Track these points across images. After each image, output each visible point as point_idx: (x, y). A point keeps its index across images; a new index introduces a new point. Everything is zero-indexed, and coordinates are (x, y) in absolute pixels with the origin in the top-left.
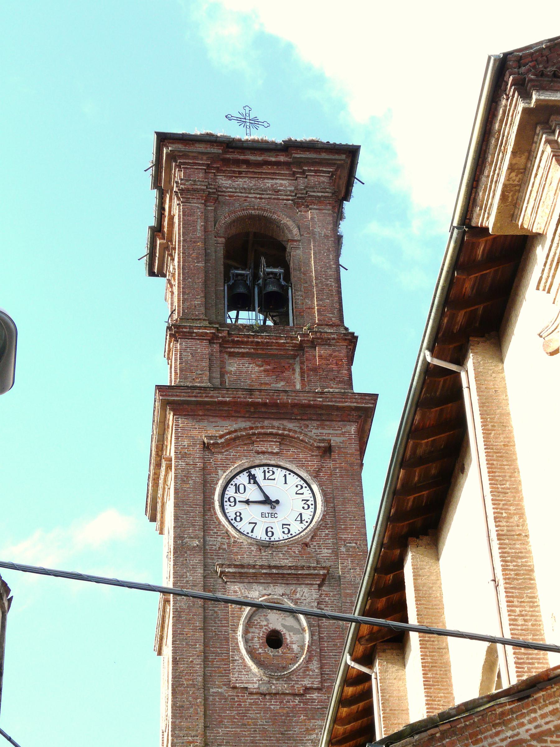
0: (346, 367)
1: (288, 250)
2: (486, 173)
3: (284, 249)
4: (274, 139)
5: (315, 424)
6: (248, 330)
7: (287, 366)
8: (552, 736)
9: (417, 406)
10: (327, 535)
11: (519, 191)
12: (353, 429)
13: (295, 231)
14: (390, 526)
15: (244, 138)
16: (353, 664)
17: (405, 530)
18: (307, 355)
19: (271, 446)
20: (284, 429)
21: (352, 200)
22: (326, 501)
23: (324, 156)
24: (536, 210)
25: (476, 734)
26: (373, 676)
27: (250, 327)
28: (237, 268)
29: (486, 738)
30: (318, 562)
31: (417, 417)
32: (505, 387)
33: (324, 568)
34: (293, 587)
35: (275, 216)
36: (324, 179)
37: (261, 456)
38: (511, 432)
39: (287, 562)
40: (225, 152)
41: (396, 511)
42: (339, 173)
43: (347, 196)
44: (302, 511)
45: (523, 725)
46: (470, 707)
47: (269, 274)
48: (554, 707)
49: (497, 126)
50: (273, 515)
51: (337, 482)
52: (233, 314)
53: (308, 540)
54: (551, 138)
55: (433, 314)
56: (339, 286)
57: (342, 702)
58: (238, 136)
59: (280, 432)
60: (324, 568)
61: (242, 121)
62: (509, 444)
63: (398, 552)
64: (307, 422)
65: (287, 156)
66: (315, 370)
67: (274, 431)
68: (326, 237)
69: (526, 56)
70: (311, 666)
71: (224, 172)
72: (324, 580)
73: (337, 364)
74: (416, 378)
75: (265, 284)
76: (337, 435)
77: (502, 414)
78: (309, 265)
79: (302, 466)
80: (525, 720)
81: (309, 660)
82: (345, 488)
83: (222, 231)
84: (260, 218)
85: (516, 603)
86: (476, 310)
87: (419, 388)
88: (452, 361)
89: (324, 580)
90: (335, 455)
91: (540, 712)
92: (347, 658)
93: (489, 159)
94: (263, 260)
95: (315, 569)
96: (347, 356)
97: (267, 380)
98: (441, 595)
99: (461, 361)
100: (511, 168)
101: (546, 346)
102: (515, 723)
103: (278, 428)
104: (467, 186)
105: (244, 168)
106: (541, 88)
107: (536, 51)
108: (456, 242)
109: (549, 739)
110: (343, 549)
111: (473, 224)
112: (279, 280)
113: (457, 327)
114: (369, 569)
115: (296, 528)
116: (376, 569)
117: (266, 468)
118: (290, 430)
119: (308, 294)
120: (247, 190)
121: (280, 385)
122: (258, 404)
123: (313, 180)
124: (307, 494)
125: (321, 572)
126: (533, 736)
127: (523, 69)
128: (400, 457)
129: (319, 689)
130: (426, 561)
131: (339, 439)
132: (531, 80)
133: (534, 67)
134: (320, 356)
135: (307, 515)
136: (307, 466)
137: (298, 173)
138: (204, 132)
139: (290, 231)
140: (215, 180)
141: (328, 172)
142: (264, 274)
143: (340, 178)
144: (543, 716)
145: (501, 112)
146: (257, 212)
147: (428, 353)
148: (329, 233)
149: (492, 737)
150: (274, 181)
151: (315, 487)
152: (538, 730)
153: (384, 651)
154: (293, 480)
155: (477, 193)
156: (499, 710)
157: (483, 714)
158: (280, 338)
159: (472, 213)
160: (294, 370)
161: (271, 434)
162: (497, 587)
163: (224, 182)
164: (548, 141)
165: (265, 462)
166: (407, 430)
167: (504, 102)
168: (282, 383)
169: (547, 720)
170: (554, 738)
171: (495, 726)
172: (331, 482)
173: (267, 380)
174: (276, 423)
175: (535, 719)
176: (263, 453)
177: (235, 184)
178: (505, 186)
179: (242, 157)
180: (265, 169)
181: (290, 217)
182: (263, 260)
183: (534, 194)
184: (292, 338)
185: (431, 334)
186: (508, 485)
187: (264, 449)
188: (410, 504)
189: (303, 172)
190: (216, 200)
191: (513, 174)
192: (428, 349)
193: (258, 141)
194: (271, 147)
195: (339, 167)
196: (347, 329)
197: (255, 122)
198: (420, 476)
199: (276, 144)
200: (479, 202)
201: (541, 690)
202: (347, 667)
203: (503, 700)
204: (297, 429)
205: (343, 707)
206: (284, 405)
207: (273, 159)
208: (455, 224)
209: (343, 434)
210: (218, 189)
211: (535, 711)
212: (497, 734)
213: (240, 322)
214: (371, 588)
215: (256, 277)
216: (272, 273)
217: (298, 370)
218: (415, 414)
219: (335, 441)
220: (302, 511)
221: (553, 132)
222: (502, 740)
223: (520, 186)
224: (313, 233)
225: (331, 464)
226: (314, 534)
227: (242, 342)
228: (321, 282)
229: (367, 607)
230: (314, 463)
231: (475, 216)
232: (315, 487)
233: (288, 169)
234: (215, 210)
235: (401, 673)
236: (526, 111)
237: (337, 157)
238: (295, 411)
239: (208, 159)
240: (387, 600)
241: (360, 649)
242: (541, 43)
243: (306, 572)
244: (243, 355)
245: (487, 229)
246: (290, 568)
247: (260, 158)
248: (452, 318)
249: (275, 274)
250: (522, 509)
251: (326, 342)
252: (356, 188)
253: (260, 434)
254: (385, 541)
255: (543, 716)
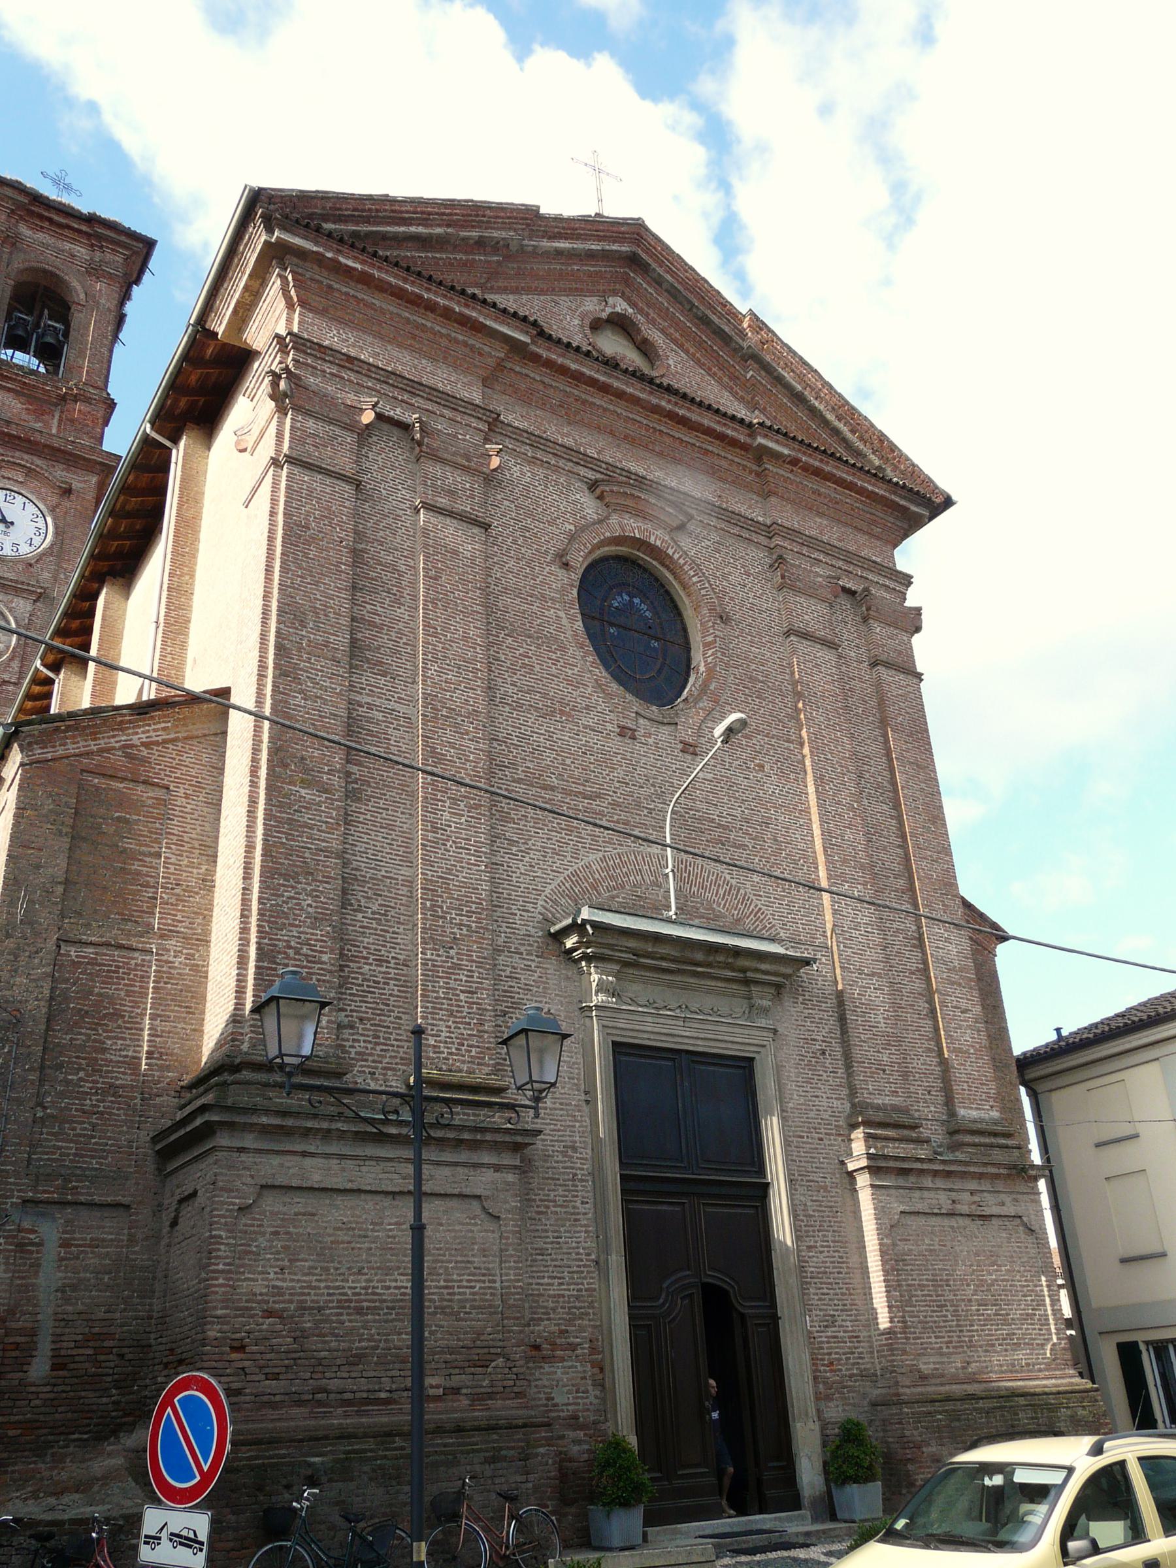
0: (100, 426)
1: (72, 310)
2: (225, 286)
3: (70, 308)
4: (80, 208)
5: (62, 466)
6: (18, 370)
7: (48, 411)
8: (158, 746)
9: (132, 467)
10: (51, 561)
11: (249, 310)
12: (94, 479)
13: (82, 296)
14: (92, 563)
15: (53, 197)
16: (42, 668)
17: (105, 569)
18: (68, 406)
19: (17, 475)
20: (32, 464)
21: (141, 286)
22: (57, 533)
23: (123, 238)
24: (259, 329)
25: (96, 733)
26: (57, 681)
27: (21, 368)
28: (21, 312)
29: (103, 738)
30: (37, 582)
31: (131, 478)
32: (206, 472)
33: (42, 588)
34: (10, 597)
35: (67, 277)
36: (119, 259)
37: (7, 481)
38: (201, 508)
39: (11, 576)
40: (31, 204)
41: (99, 552)
42: (133, 258)
43: (137, 281)
44: (34, 537)
45: (137, 733)
46: (96, 711)
47: (49, 326)
48: (167, 725)
49: (241, 248)
50: (6, 534)
51: (70, 519)
52: (9, 352)
53: (33, 562)
54: (282, 273)
55: (159, 394)
56: (111, 356)
57: (28, 696)
58: (46, 194)
59: (28, 465)
60: (42, 588)
61: (56, 182)
62: (197, 518)
63: (96, 586)
64: (55, 463)
65: (89, 227)
66: (72, 421)
67: (23, 463)
68: (109, 310)
69: (277, 196)
70: (12, 664)
71: (26, 221)
72: (39, 597)
73: (93, 422)
74: (135, 444)
75: (43, 335)
76: (79, 481)
77: (197, 492)
78: (88, 330)
79: (42, 499)
80: (140, 731)
81: (11, 659)
82: (75, 527)
83: (13, 275)
84: (53, 274)
85: (169, 644)
86: (198, 401)
87: (136, 454)
88: (169, 439)
89: (39, 597)
90: (73, 497)
91: (153, 727)
92: (38, 663)
93: (230, 275)
94: (46, 312)
95: (33, 586)
96: (104, 417)
97: (27, 417)
98: (123, 628)
99: (175, 441)
100: (246, 288)
101: (237, 443)
102: (131, 731)
103: (27, 461)
104: (208, 292)
105: (46, 224)
106: (284, 228)
107: (286, 196)
108: (189, 338)
109: (155, 748)
110: (62, 576)
111: (207, 327)
112: (58, 334)
113: (179, 411)
114: (68, 594)
115: (24, 549)
116: (74, 595)
117: (8, 492)
118: (37, 466)
119: (82, 354)
120: (46, 246)
121: (38, 425)
122: (13, 436)
123: (109, 256)
124: (41, 523)
125: (39, 591)
126: (143, 744)
127: (272, 207)
128: (111, 506)
129: (15, 684)
130: (117, 599)
131: (80, 485)
132: (276, 218)
133: (282, 208)
134: (80, 411)
135: (37, 541)
136: (46, 501)
137: (97, 246)
138: (14, 178)
139: (78, 295)
140: (16, 227)
141: (124, 255)
142: (45, 325)
143: (134, 263)
144: (155, 730)
145: (247, 237)
146: (50, 268)
147: (148, 426)
148: (113, 308)
149: (108, 737)
150: (73, 246)
151: (49, 519)
152: (148, 740)
153: (71, 663)
154: (31, 508)
155: (215, 301)
156: (119, 719)
157: (105, 720)
158: (47, 385)
159: (208, 317)
160: (53, 416)
161: (19, 464)
162: (157, 627)
163: (24, 230)
164: (279, 275)
165: (8, 486)
166: (121, 486)
167: (251, 230)
168: (40, 424)
169: (158, 733)
170: (160, 748)
171: (113, 730)
172: (65, 518)
173: (27, 417)
174: (26, 457)
175: (148, 731)
176: (9, 479)
177: (35, 236)
178: (238, 302)
179: (46, 214)
180: (66, 232)
181: (80, 282)
182: (46, 312)
183: (260, 316)
184: (57, 388)
185: (154, 411)
186: (187, 550)
187: (10, 476)
188: (113, 549)
189: (101, 247)
190: (13, 244)
191: (247, 294)
192: (150, 422)
193: (64, 205)
194: (77, 214)
195: (135, 253)
196: (108, 394)
197: (68, 188)
198: (125, 527)
199: (81, 213)
200: (215, 309)
201: (159, 710)
202: (37, 670)
203: (124, 712)
204: (44, 466)
205: (29, 700)
206: (37, 443)
207: (76, 226)
208: (192, 322)
209: (85, 481)
210: (17, 235)
211: (149, 725)
212: (114, 736)
213: (14, 360)
214: (68, 610)
215: (37, 325)
216: (53, 326)
217: (57, 417)
218: (129, 474)
219: (76, 485)
220: (34, 537)
221: (286, 269)
222: (117, 742)
223: (251, 306)
224: (98, 303)
225: (68, 504)
226: (40, 557)
227: (10, 378)
228: (96, 348)
229: (62, 625)
230: (54, 499)
231: (210, 319)
232: (49, 519)
233: (88, 240)
234: (11, 253)
235: (81, 683)
236: (267, 243)
237: (135, 243)
238: (46, 450)
239: (13, 204)
240: (81, 623)
241: (51, 658)
242: (293, 190)
243: (25, 587)
244: (9, 390)
245: (217, 334)
246: (11, 580)
247: (64, 221)
248: (176, 402)
249: (56, 328)
250: (194, 571)
251: (88, 400)
252: (147, 277)
253: (9, 461)
254: (86, 574)
255: (155, 730)
